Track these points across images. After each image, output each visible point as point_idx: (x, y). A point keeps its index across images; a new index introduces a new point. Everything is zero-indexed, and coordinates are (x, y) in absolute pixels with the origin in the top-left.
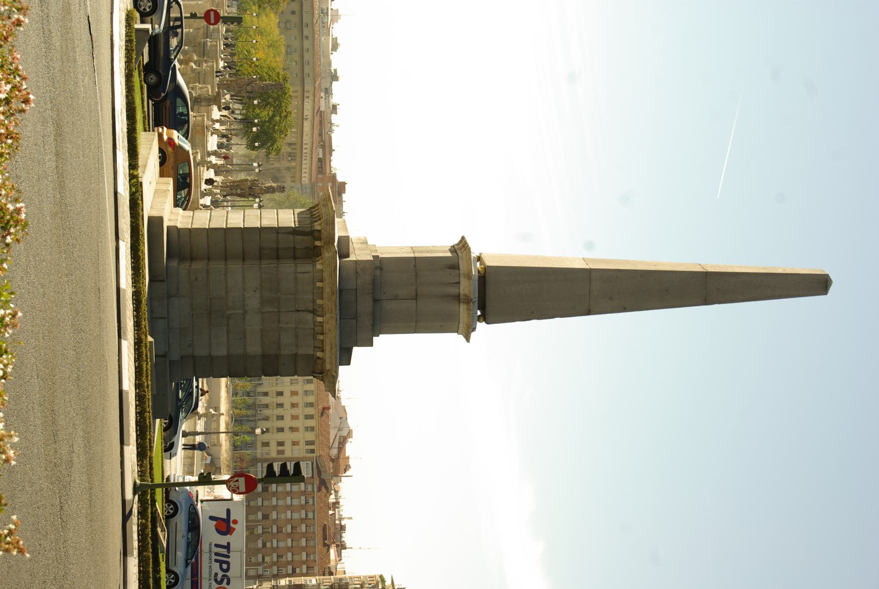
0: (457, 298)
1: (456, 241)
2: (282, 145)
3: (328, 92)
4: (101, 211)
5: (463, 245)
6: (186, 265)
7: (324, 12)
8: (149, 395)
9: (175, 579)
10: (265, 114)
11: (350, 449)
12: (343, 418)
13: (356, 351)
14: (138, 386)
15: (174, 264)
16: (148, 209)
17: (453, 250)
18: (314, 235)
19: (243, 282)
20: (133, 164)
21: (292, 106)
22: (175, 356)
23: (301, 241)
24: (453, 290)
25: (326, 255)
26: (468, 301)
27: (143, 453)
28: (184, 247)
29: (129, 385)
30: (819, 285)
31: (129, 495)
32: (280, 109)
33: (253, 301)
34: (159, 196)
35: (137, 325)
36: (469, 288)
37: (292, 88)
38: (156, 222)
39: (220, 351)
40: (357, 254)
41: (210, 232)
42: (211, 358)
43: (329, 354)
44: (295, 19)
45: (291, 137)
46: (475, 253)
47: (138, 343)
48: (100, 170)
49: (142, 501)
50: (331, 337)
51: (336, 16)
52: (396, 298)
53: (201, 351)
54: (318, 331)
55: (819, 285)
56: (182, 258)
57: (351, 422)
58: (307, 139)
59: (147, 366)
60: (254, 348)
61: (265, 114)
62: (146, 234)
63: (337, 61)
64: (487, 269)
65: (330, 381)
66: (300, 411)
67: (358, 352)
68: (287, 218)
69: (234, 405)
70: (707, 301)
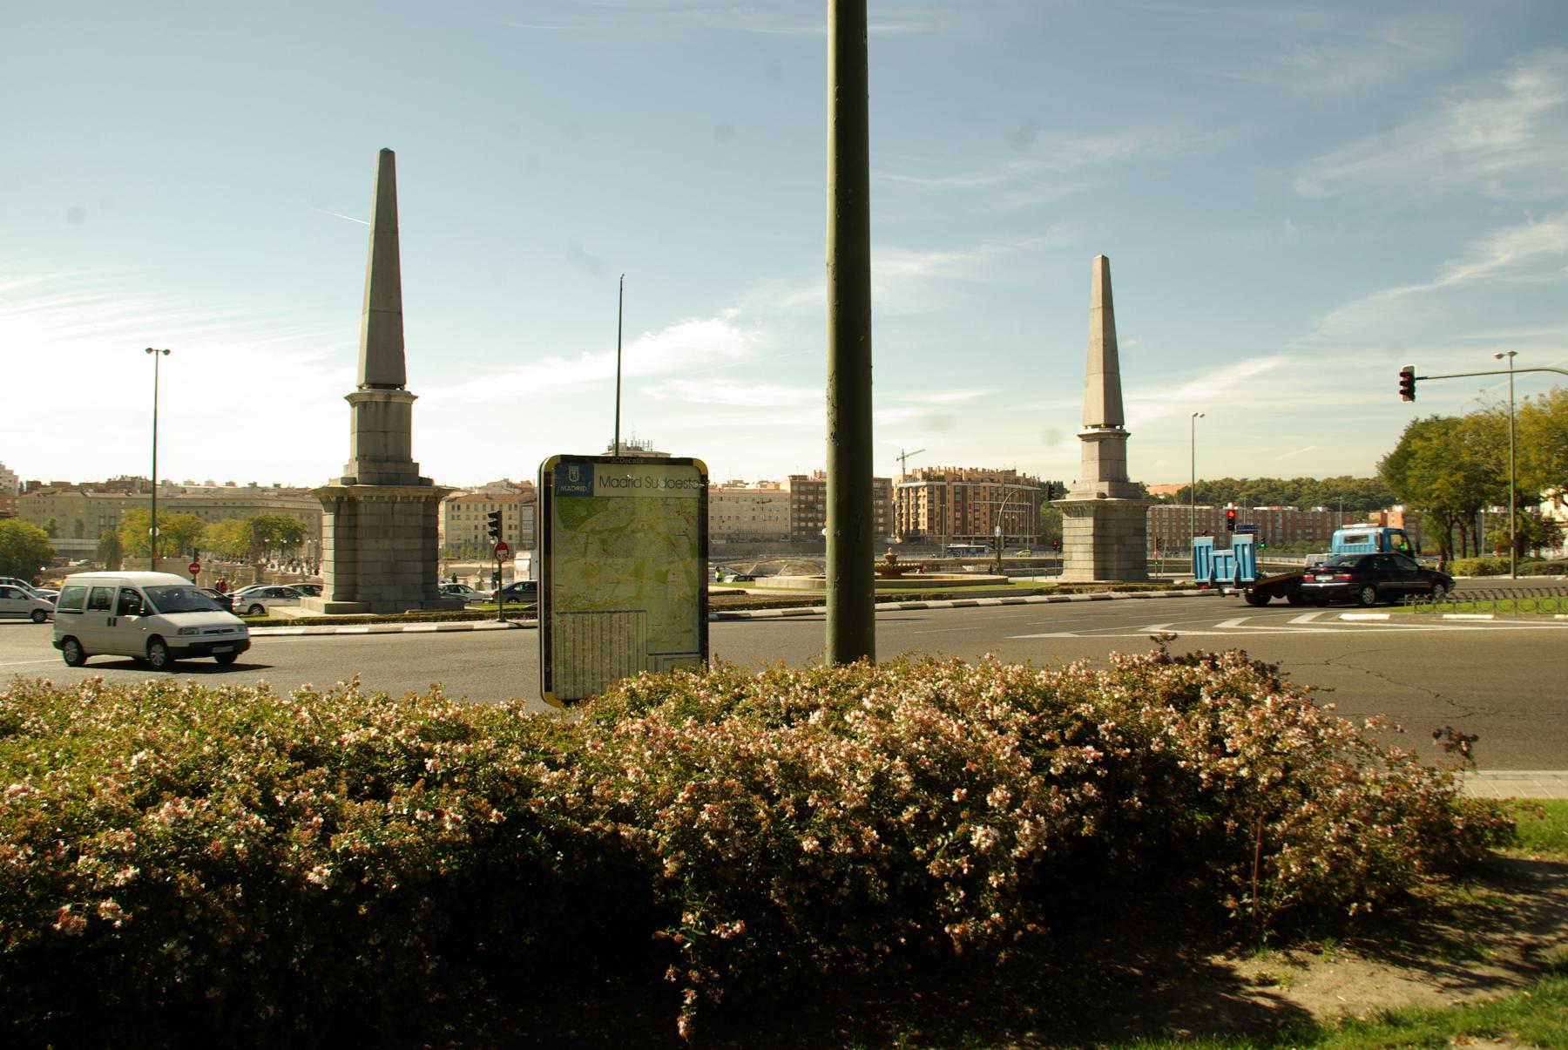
0: (387, 403)
1: (347, 403)
2: (297, 520)
3: (264, 490)
4: (319, 645)
5: (350, 398)
6: (361, 590)
7: (207, 491)
8: (435, 614)
9: (4, 593)
10: (277, 534)
11: (516, 480)
12: (494, 485)
13: (422, 474)
14: (435, 620)
15: (358, 597)
16: (320, 614)
17: (353, 405)
18: (340, 501)
19: (372, 550)
20: (294, 623)
21: (272, 515)
22: (422, 597)
23: (344, 510)
24: (381, 406)
25: (353, 493)
26: (389, 396)
27: (480, 616)
28: (346, 589)
29: (433, 626)
30: (387, 158)
31: (505, 625)
32: (269, 524)
33: (386, 544)
34: (313, 607)
35: (394, 621)
36: (380, 396)
37: (260, 515)
38: (329, 609)
39: (419, 566)
40: (354, 473)
41: (337, 572)
42: (424, 573)
43: (424, 493)
44: (211, 512)
45: (296, 517)
46: (356, 390)
47: (407, 620)
48: (281, 645)
49: (511, 617)
50: (411, 491)
51: (210, 483)
52: (386, 446)
53: (419, 579)
54: (407, 500)
55: (387, 158)
56: (355, 592)
57: (497, 479)
58: (297, 506)
59: (424, 614)
60: (418, 543)
61: (277, 534)
62: (337, 614)
63: (242, 483)
64: (367, 383)
65: (443, 492)
66: (472, 515)
67: (423, 473)
68: (328, 520)
69: (483, 558)
70: (396, 232)
